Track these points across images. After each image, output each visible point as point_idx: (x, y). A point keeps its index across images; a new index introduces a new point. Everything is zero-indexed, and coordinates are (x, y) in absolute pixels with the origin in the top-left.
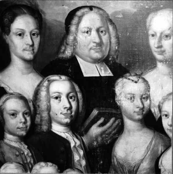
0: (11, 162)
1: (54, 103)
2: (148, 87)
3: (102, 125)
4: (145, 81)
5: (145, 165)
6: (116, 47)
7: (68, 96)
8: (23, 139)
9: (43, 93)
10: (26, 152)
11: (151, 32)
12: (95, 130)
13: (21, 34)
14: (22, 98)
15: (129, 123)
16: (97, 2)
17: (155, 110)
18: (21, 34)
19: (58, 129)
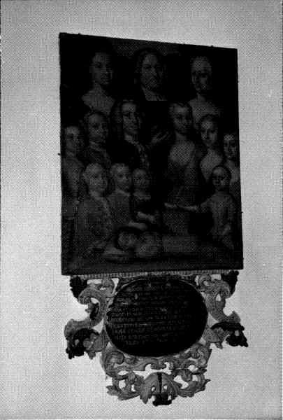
0: (95, 162)
1: (125, 119)
2: (190, 110)
3: (159, 137)
4: (189, 106)
5: (192, 165)
6: (100, 299)
7: (135, 114)
8: (102, 145)
9: (117, 112)
10: (105, 155)
11: (192, 72)
12: (155, 140)
13: (100, 66)
14: (100, 113)
15: (178, 135)
16: (181, 357)
17: (196, 127)
18: (100, 66)
19: (128, 138)
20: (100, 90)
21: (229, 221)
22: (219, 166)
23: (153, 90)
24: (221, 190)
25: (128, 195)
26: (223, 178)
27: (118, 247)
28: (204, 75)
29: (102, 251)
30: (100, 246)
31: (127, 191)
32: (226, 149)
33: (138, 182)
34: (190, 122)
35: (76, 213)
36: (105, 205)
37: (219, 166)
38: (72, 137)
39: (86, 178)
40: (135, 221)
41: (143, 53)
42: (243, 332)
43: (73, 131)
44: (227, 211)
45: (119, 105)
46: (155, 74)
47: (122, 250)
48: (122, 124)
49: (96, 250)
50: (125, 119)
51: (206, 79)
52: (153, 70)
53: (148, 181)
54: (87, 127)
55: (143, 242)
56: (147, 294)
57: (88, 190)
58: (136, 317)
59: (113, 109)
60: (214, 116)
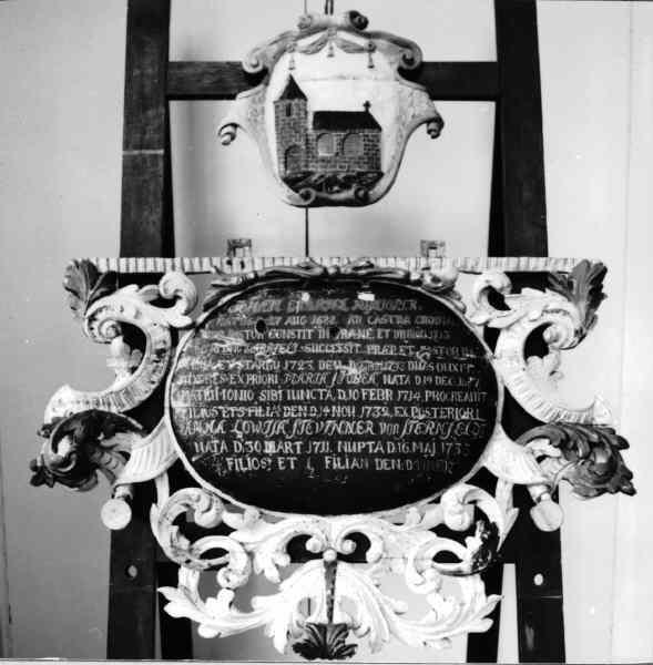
56: (301, 395)
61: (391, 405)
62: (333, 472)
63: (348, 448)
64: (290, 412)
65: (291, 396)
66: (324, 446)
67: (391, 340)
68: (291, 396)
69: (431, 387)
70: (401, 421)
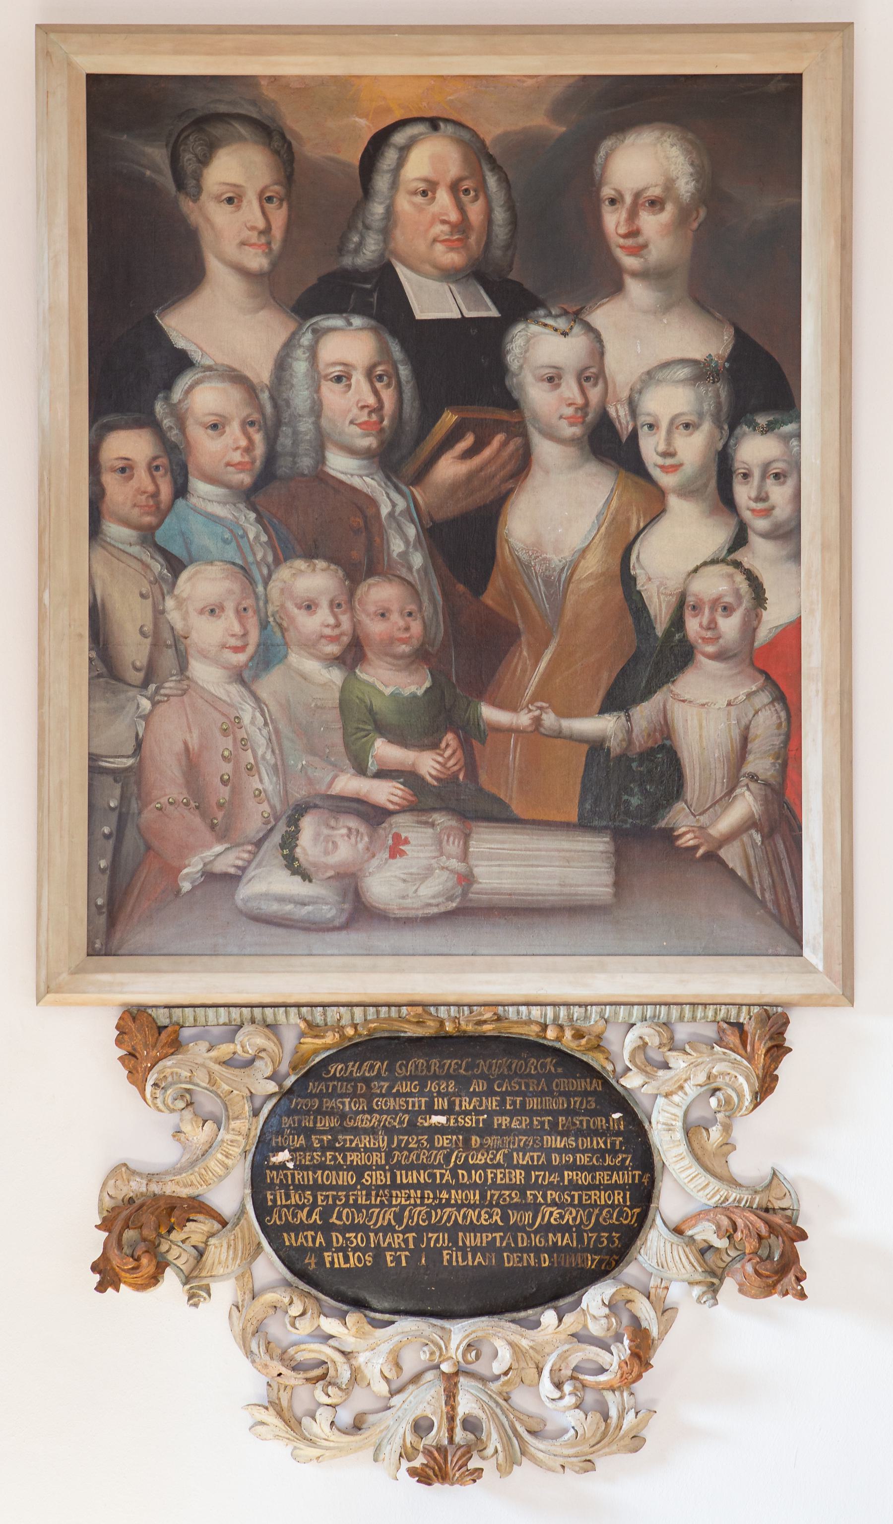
1: (331, 394)
4: (589, 329)
7: (370, 374)
9: (300, 367)
10: (253, 530)
11: (607, 192)
14: (237, 378)
17: (619, 413)
20: (720, 1127)
21: (753, 777)
22: (713, 562)
23: (449, 275)
24: (720, 656)
25: (336, 676)
26: (728, 610)
27: (293, 866)
28: (656, 204)
29: (232, 879)
30: (227, 863)
31: (339, 660)
32: (743, 493)
33: (376, 628)
34: (595, 394)
35: (139, 744)
36: (248, 713)
37: (713, 562)
38: (126, 469)
39: (174, 617)
40: (361, 770)
41: (399, 138)
42: (798, 1245)
43: (780, 77)
44: (745, 740)
45: (306, 339)
46: (454, 216)
47: (306, 877)
48: (317, 409)
49: (210, 877)
50: (331, 394)
51: (667, 215)
52: (443, 197)
53: (416, 627)
54: (182, 428)
55: (395, 852)
56: (413, 1177)
57: (183, 666)
58: (359, 1170)
59: (282, 365)
60: (695, 362)
61: (522, 1190)
62: (450, 1268)
63: (471, 1240)
64: (400, 1197)
65: (402, 1177)
66: (444, 1239)
67: (523, 1111)
68: (402, 1177)
69: (573, 1167)
70: (536, 1208)
